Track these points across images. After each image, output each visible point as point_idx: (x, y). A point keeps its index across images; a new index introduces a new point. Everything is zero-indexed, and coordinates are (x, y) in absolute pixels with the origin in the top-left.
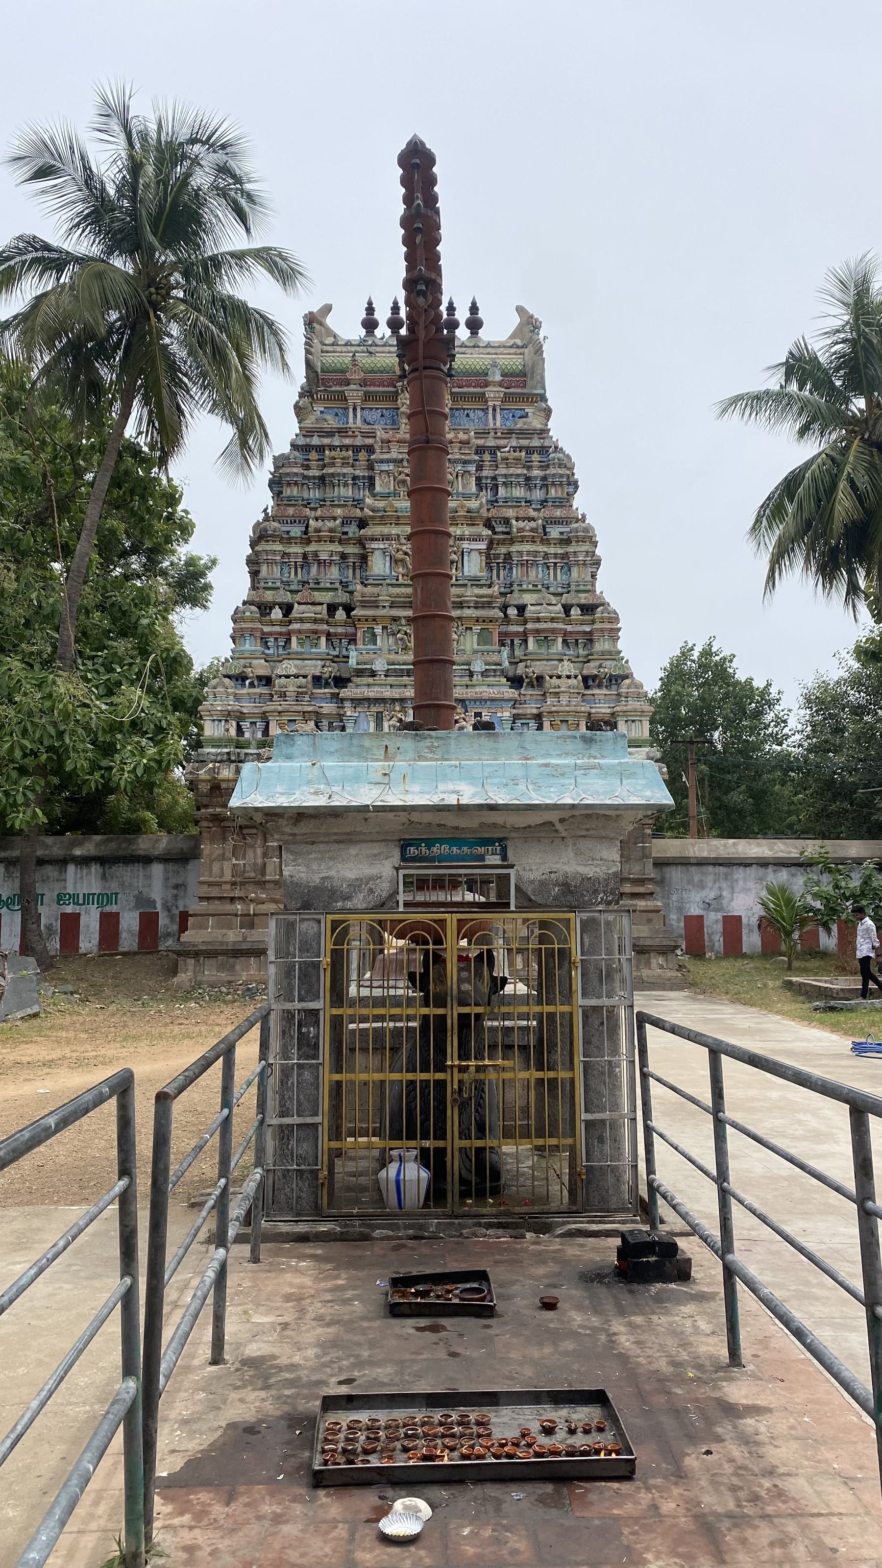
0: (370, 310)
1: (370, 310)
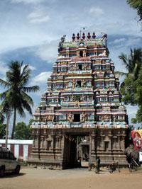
0: (74, 35)
1: (74, 35)
